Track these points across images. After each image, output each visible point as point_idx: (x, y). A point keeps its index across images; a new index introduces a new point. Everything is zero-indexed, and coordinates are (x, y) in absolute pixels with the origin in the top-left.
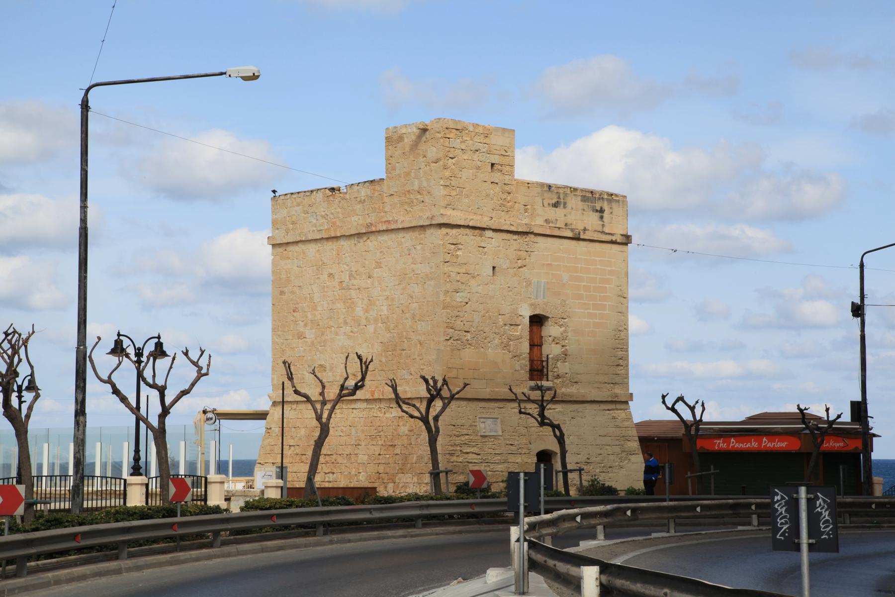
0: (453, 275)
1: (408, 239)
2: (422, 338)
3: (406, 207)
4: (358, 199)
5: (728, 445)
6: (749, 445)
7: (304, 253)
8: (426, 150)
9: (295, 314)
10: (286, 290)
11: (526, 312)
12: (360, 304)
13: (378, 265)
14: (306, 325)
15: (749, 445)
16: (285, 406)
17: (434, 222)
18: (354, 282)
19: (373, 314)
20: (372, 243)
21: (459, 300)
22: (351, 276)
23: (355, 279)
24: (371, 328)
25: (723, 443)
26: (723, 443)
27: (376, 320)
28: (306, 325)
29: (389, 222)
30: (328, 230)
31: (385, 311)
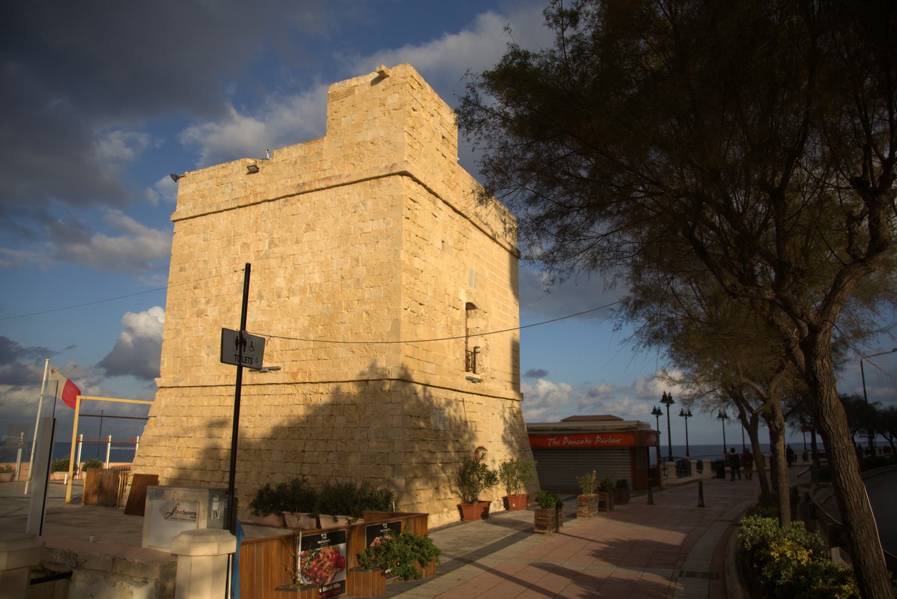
0: (413, 235)
1: (352, 194)
2: (370, 307)
3: (352, 161)
4: (287, 162)
5: (561, 442)
6: (582, 442)
7: (213, 226)
8: (386, 98)
9: (196, 291)
10: (187, 265)
11: (464, 299)
12: (281, 272)
13: (310, 228)
14: (208, 302)
15: (582, 442)
16: (667, 444)
17: (395, 171)
18: (275, 250)
19: (299, 282)
20: (303, 204)
21: (416, 266)
22: (272, 243)
23: (276, 246)
24: (296, 300)
25: (556, 440)
26: (556, 440)
27: (303, 290)
28: (208, 302)
29: (329, 178)
30: (247, 197)
31: (317, 278)
